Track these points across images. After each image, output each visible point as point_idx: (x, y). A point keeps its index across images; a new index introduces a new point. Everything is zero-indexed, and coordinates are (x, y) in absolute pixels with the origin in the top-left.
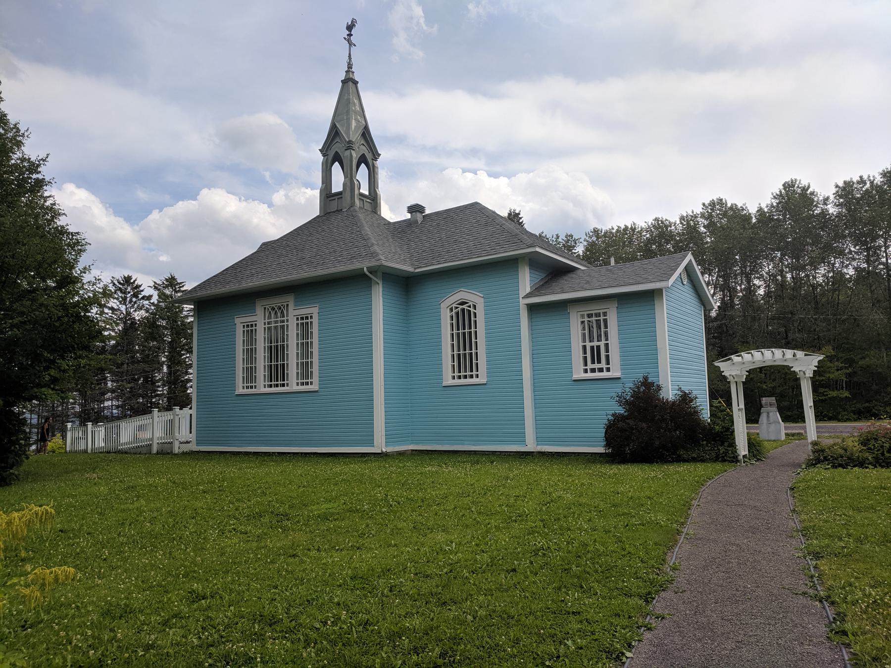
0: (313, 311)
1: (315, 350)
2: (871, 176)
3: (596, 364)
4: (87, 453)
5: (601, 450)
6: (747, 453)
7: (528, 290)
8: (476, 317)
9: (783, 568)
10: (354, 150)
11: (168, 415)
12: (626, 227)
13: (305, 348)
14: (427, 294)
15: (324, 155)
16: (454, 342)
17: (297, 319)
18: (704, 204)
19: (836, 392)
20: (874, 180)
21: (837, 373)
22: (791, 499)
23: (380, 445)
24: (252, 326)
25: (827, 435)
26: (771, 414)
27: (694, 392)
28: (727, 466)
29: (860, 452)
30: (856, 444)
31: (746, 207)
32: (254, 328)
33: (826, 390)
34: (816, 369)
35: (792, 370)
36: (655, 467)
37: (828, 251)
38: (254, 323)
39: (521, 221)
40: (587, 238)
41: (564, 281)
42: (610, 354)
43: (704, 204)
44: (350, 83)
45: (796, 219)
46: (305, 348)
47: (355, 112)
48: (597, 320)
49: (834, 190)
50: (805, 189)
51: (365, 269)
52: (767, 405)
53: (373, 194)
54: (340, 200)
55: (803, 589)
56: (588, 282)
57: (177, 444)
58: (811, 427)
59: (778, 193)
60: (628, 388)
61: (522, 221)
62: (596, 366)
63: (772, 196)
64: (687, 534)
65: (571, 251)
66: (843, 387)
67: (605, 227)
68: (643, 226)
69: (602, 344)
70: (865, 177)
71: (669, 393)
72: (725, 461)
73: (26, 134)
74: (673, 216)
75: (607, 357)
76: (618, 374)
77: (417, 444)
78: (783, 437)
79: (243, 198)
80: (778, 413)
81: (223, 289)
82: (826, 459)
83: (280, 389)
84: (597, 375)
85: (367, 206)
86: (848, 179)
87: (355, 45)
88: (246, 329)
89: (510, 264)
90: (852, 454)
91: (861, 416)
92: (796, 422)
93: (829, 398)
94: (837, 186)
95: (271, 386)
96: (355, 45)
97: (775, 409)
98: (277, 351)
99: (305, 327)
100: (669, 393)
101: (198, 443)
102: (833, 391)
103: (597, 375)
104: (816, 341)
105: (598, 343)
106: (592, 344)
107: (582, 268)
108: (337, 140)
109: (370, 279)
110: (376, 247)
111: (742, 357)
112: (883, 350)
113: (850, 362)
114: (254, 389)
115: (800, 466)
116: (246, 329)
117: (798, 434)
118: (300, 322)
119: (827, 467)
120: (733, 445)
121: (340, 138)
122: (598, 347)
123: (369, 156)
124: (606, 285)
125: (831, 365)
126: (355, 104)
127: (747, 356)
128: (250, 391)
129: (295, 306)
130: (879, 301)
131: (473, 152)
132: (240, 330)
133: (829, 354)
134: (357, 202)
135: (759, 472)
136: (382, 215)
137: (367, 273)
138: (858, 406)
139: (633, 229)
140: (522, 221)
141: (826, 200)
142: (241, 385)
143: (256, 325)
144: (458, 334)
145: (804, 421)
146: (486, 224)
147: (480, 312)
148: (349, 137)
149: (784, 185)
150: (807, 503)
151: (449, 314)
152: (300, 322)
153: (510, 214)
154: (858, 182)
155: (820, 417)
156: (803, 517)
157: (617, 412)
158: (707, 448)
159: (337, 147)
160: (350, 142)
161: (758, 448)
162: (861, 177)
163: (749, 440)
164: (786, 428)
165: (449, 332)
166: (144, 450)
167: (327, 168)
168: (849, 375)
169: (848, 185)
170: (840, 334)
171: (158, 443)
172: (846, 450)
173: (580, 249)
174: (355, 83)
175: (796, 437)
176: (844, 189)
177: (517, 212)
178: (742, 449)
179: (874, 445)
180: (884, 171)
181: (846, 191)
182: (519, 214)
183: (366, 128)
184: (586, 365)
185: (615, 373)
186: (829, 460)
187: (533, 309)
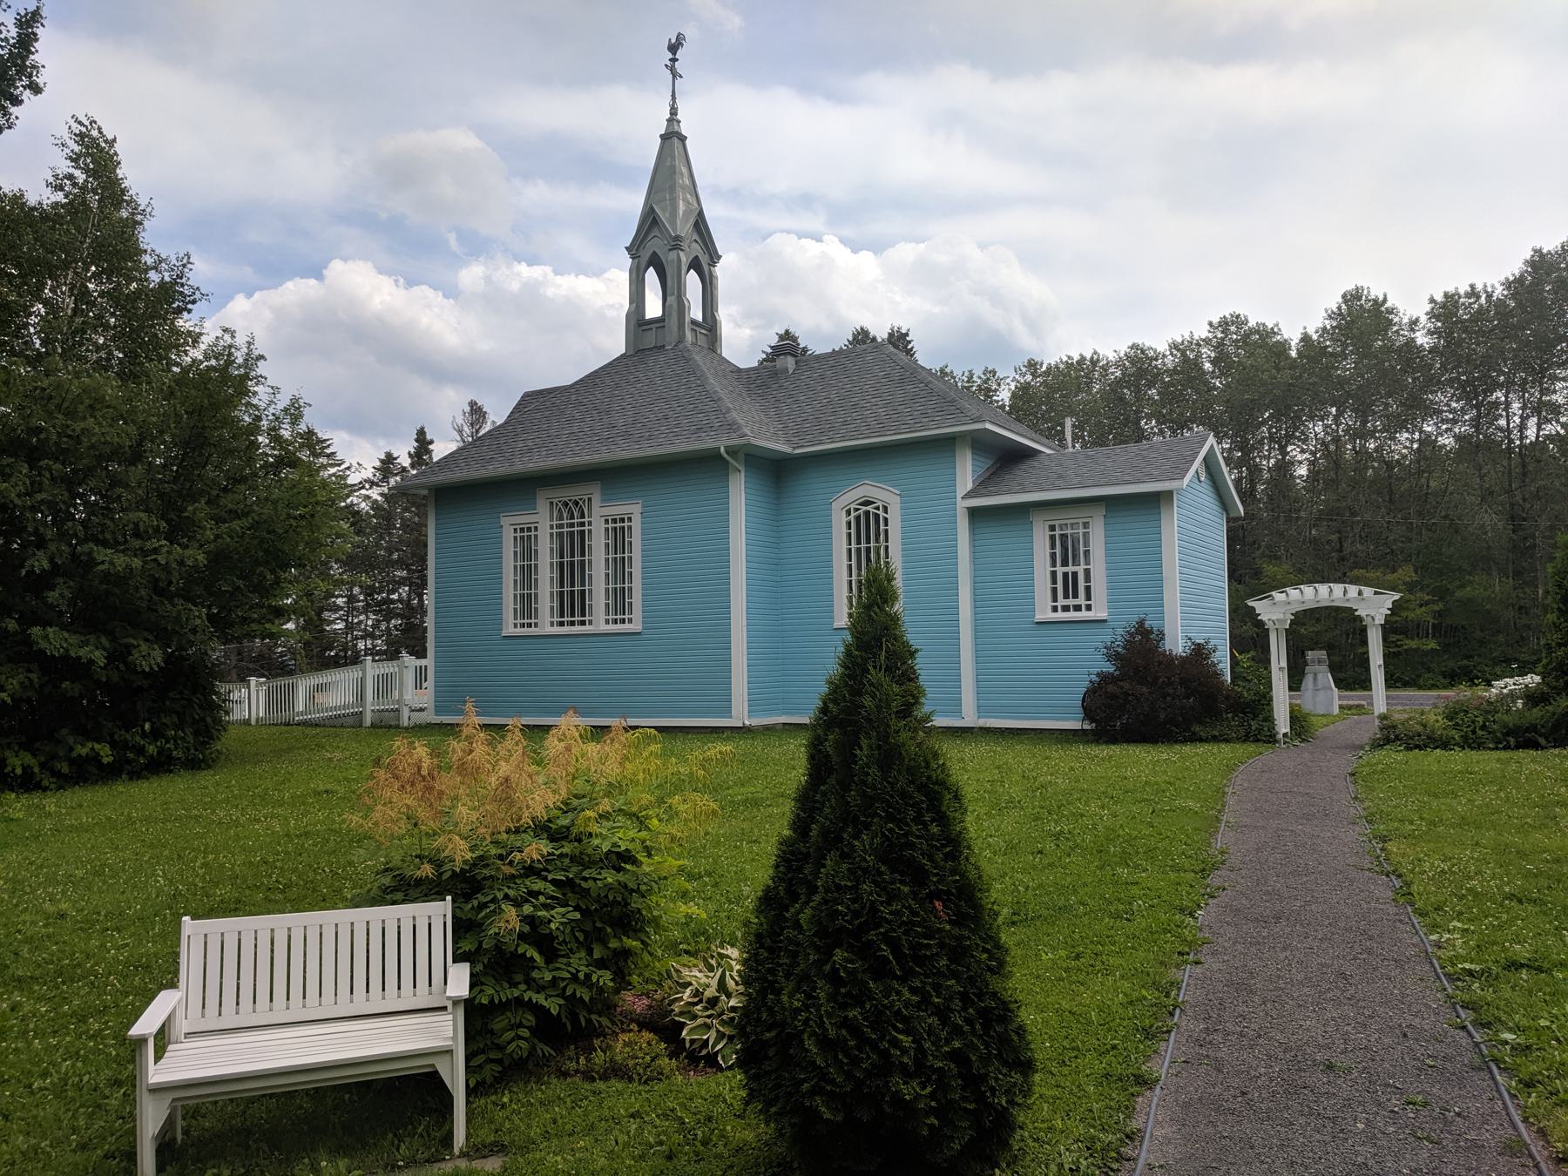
0: (634, 509)
1: (637, 569)
2: (1488, 285)
3: (1071, 599)
4: (250, 724)
5: (1075, 725)
6: (1288, 730)
7: (970, 486)
8: (887, 525)
9: (1346, 850)
10: (682, 250)
11: (389, 668)
12: (1083, 358)
13: (620, 568)
14: (812, 487)
15: (633, 257)
16: (853, 562)
17: (607, 521)
18: (1211, 324)
19: (1416, 641)
20: (1493, 292)
21: (1419, 611)
22: (1351, 787)
23: (740, 714)
24: (529, 529)
25: (1400, 708)
26: (1320, 676)
27: (1213, 642)
28: (1262, 747)
29: (1444, 729)
30: (1440, 718)
31: (1279, 329)
32: (533, 533)
33: (1400, 637)
34: (1389, 612)
35: (1356, 613)
36: (1162, 748)
37: (1416, 408)
38: (532, 526)
39: (909, 347)
40: (1017, 377)
41: (1022, 472)
42: (1091, 584)
43: (1211, 324)
44: (676, 140)
45: (1364, 352)
46: (620, 568)
47: (683, 188)
48: (1062, 535)
49: (1428, 307)
50: (1378, 304)
51: (722, 449)
52: (1314, 662)
53: (709, 320)
54: (659, 330)
55: (1369, 866)
56: (1060, 477)
57: (406, 713)
58: (1379, 696)
59: (1335, 310)
60: (1115, 635)
61: (912, 348)
62: (1071, 602)
63: (1325, 315)
64: (1227, 822)
65: (991, 397)
66: (1428, 634)
67: (1052, 355)
68: (1111, 358)
69: (1080, 570)
70: (1479, 287)
71: (1177, 644)
72: (1258, 741)
73: (148, 210)
74: (1159, 342)
75: (1088, 589)
76: (1103, 615)
77: (792, 714)
78: (1336, 711)
79: (402, 280)
80: (1329, 675)
81: (484, 472)
82: (1397, 738)
83: (577, 629)
84: (1072, 615)
85: (702, 341)
86: (1451, 290)
87: (681, 76)
88: (518, 534)
89: (946, 444)
90: (1433, 731)
91: (1454, 680)
92: (1351, 690)
93: (1406, 651)
94: (1432, 300)
95: (561, 624)
96: (681, 76)
97: (1325, 668)
98: (571, 572)
99: (619, 535)
100: (1177, 644)
101: (438, 711)
102: (1412, 639)
103: (1072, 615)
104: (1389, 557)
105: (1075, 569)
106: (1065, 569)
107: (1048, 451)
108: (655, 232)
109: (727, 462)
110: (734, 414)
111: (1287, 595)
112: (1495, 573)
113: (1442, 594)
114: (533, 629)
115: (1362, 748)
116: (518, 534)
117: (1358, 706)
118: (610, 525)
119: (1399, 748)
120: (1269, 719)
121: (661, 231)
122: (1075, 574)
123: (704, 260)
124: (1090, 483)
125: (1413, 598)
126: (682, 174)
127: (1293, 593)
128: (526, 631)
129: (603, 501)
130: (1491, 493)
131: (805, 201)
132: (508, 536)
133: (1408, 579)
134: (689, 335)
135: (1306, 755)
136: (724, 355)
137: (725, 455)
138: (1451, 664)
139: (1094, 362)
140: (912, 348)
141: (1414, 323)
142: (511, 621)
143: (536, 528)
144: (859, 551)
145: (1371, 690)
146: (902, 381)
147: (895, 517)
148: (675, 231)
149: (1344, 296)
150: (1372, 789)
151: (845, 519)
152: (610, 525)
153: (891, 335)
154: (1468, 295)
155: (1392, 682)
156: (1367, 804)
157: (1104, 670)
158: (1233, 723)
159: (655, 245)
160: (677, 238)
161: (1303, 723)
162: (1472, 287)
163: (1291, 712)
164: (1340, 698)
165: (845, 547)
166: (350, 721)
167: (638, 275)
168: (1440, 614)
169: (1451, 300)
170: (1427, 547)
171: (373, 711)
172: (1425, 726)
173: (1004, 396)
174: (683, 139)
175: (1354, 711)
176: (1444, 306)
177: (904, 331)
178: (1283, 726)
179: (1463, 720)
180: (1507, 279)
181: (1446, 310)
182: (907, 335)
183: (701, 214)
184: (1055, 600)
185: (1099, 612)
186: (1401, 739)
187: (974, 513)
